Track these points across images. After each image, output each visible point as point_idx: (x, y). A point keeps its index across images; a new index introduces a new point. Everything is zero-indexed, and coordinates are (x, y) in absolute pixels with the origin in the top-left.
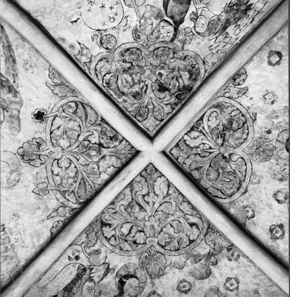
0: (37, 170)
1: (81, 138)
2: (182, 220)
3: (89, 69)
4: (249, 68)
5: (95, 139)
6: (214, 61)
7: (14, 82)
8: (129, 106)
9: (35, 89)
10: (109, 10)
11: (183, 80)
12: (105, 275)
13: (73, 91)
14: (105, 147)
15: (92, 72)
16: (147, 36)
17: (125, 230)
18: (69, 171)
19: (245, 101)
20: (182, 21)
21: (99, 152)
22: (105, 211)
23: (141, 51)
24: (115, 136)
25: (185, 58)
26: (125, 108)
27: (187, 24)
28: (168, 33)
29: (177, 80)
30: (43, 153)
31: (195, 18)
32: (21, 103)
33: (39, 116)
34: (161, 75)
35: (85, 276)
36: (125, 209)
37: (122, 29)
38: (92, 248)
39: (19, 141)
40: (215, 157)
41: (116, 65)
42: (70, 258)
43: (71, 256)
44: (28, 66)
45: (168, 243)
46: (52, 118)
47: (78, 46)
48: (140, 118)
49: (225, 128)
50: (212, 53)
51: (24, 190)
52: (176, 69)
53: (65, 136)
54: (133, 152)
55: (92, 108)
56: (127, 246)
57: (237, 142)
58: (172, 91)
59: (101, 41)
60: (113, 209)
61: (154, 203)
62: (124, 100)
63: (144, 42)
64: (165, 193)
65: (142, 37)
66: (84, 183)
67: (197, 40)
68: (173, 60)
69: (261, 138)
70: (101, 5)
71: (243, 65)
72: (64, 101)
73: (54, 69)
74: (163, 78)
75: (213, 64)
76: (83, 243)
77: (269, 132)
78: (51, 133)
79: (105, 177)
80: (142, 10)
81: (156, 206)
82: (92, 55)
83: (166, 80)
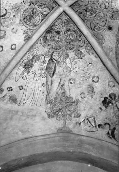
1: (94, 15)
3: (87, 44)
4: (23, 42)
5: (88, 13)
6: (37, 44)
8: (72, 26)
9: (110, 40)
10: (77, 66)
14: (84, 9)
16: (63, 55)
19: (24, 28)
20: (49, 60)
21: (87, 8)
23: (66, 48)
24: (79, 14)
25: (48, 45)
27: (47, 59)
30: (112, 13)
31: (44, 62)
34: (58, 38)
37: (73, 58)
40: (37, 3)
44: (111, 49)
46: (105, 26)
47: (91, 53)
48: (68, 20)
49: (32, 16)
50: (38, 48)
52: (52, 40)
53: (101, 17)
54: (73, 6)
55: (88, 27)
57: (27, 10)
59: (81, 54)
62: (74, 29)
65: (65, 54)
67: (43, 52)
68: (54, 44)
69: (17, 13)
70: (80, 69)
71: (26, 44)
72: (99, 32)
73: (101, 46)
74: (58, 37)
75: (38, 43)
77: (14, 16)
78: (106, 20)
80: (64, 65)
83: (56, 36)
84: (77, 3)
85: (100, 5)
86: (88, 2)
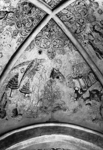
0: (57, 53)
1: (47, 38)
2: (77, 6)
3: (25, 38)
5: (47, 33)
7: (30, 62)
11: (27, 6)
12: (92, 35)
13: (32, 42)
14: (50, 29)
15: (25, 36)
17: (78, 25)
18: (58, 42)
20: (6, 11)
21: (52, 31)
22: (71, 31)
24: (47, 26)
26: (37, 23)
27: (7, 10)
28: (11, 14)
29: (27, 8)
30: (52, 51)
31: (5, 8)
32: (36, 59)
33: (40, 52)
34: (25, 14)
35: (92, 42)
36: (71, 24)
38: (83, 38)
39: (48, 59)
41: (23, 29)
42: (85, 46)
43: (85, 45)
44: (25, 58)
45: (84, 12)
46: (41, 48)
47: (18, 43)
48: (40, 18)
51: (63, 58)
52: (23, 9)
53: (47, 43)
56: (84, 26)
58: (31, 9)
59: (16, 35)
60: (71, 28)
61: (70, 14)
63: (14, 21)
64: (67, 10)
66: (62, 37)
68: (20, 11)
74: (26, 13)
76: (81, 41)
78: (45, 48)
79: (60, 30)
80: (4, 25)
81: (71, 14)
82: (20, 38)
84: (55, 23)
85: (56, 41)
86: (56, 32)
